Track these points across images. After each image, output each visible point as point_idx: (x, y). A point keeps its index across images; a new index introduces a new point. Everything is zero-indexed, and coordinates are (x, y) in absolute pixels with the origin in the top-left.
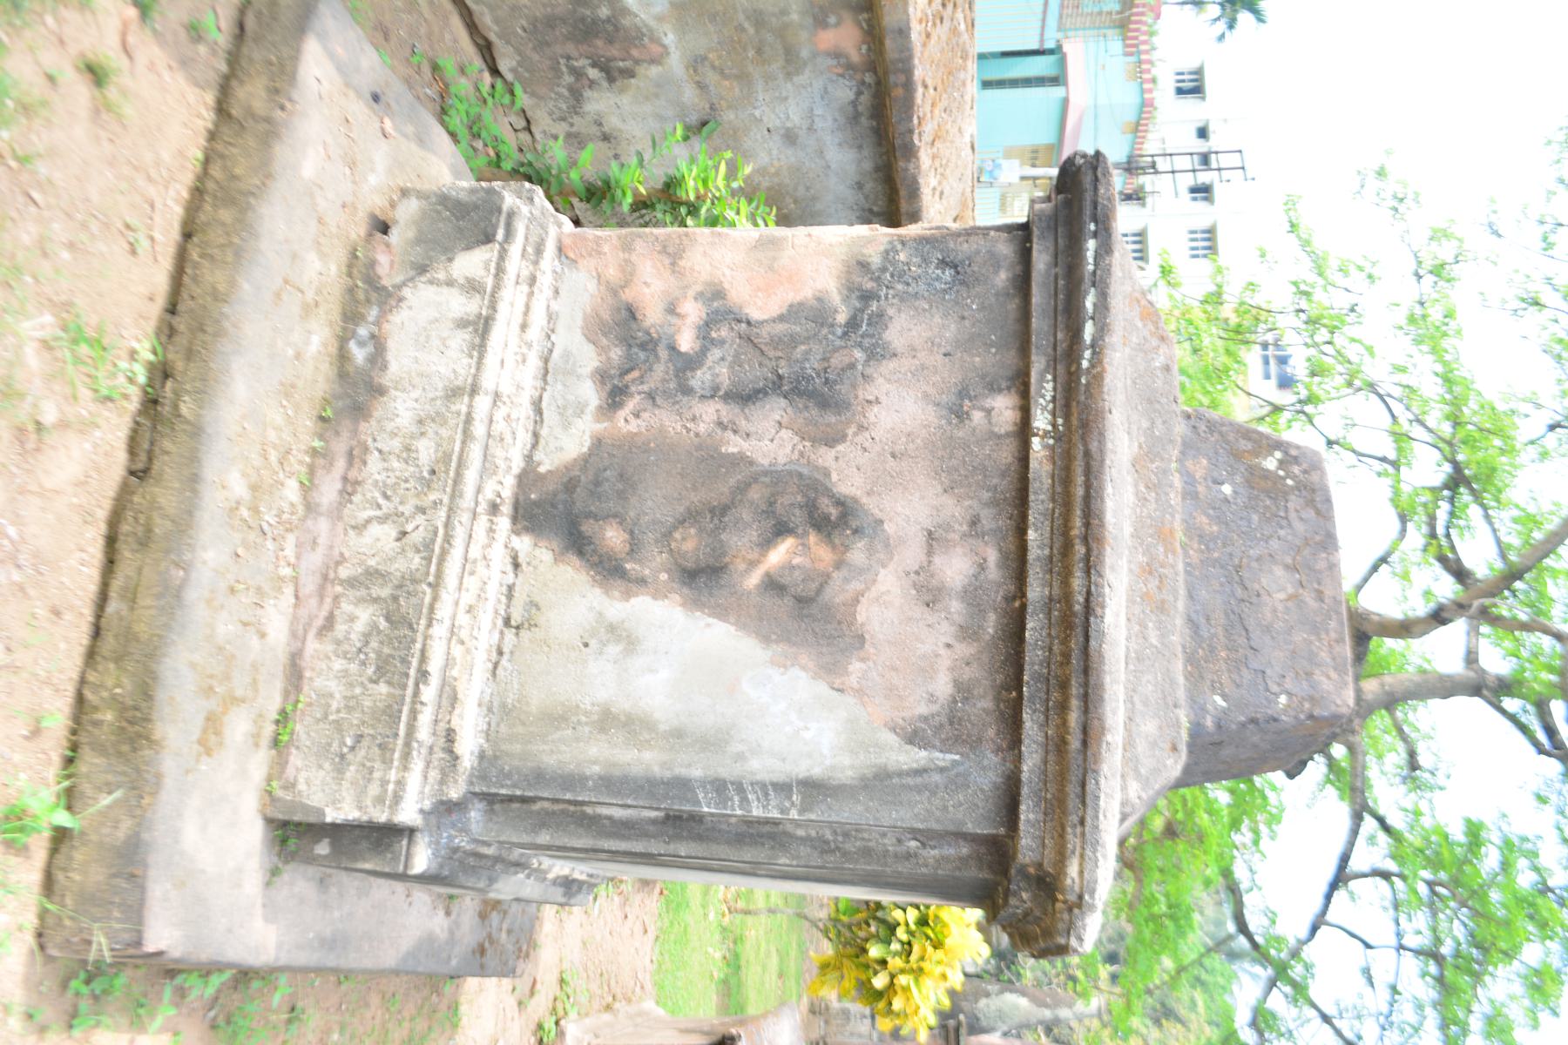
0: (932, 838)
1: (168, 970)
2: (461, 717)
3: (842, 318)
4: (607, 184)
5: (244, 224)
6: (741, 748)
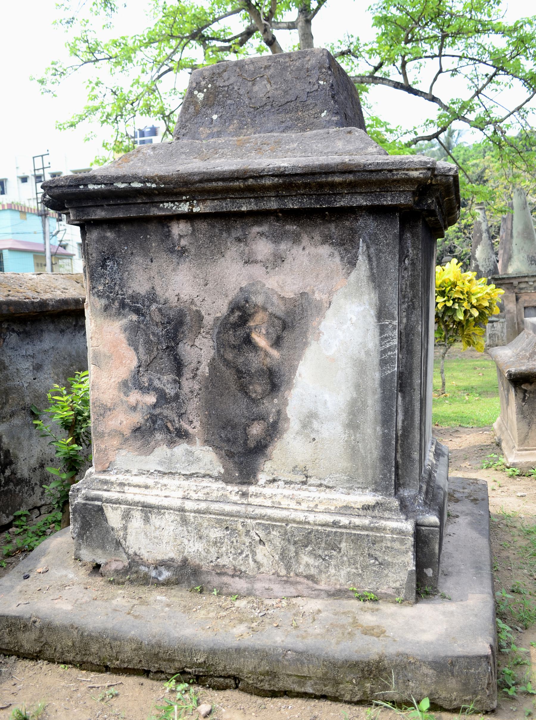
0: (403, 252)
1: (498, 649)
2: (355, 503)
3: (135, 317)
4: (66, 459)
5: (98, 638)
6: (363, 353)
